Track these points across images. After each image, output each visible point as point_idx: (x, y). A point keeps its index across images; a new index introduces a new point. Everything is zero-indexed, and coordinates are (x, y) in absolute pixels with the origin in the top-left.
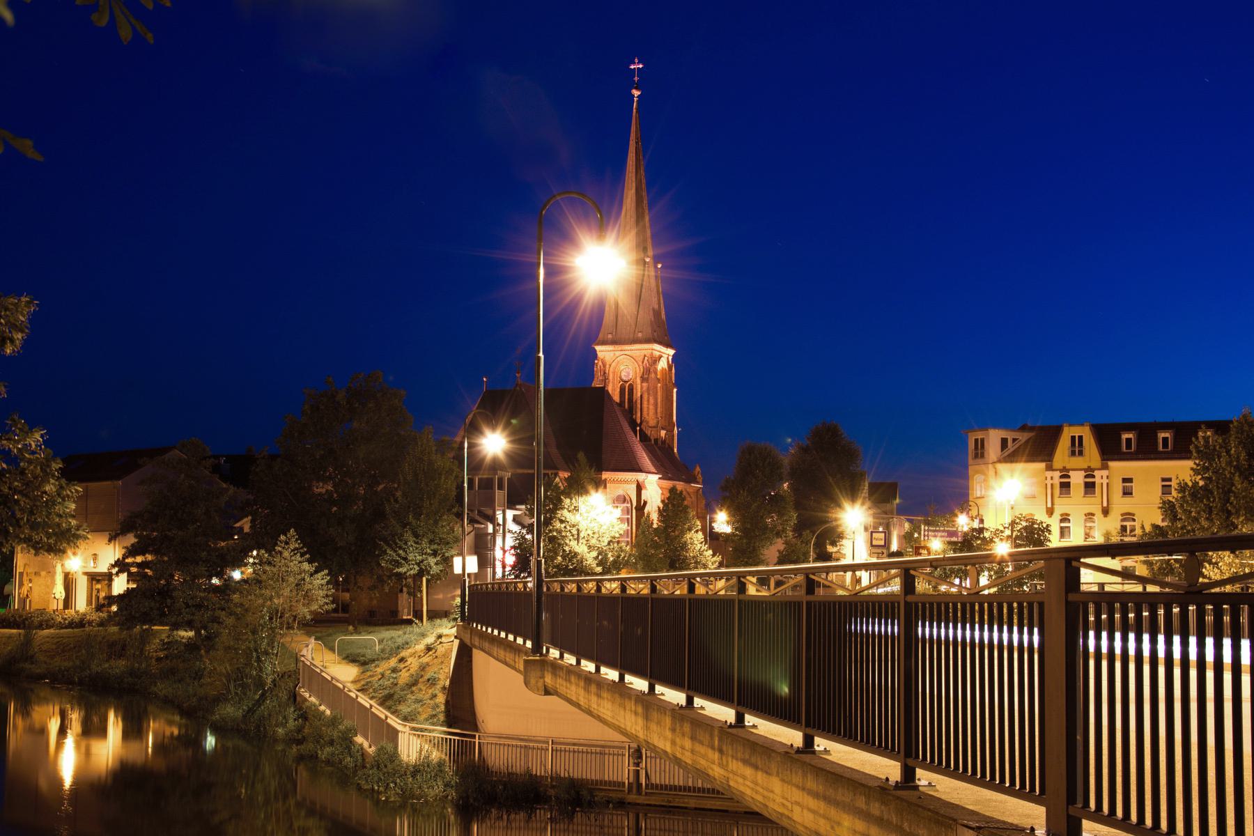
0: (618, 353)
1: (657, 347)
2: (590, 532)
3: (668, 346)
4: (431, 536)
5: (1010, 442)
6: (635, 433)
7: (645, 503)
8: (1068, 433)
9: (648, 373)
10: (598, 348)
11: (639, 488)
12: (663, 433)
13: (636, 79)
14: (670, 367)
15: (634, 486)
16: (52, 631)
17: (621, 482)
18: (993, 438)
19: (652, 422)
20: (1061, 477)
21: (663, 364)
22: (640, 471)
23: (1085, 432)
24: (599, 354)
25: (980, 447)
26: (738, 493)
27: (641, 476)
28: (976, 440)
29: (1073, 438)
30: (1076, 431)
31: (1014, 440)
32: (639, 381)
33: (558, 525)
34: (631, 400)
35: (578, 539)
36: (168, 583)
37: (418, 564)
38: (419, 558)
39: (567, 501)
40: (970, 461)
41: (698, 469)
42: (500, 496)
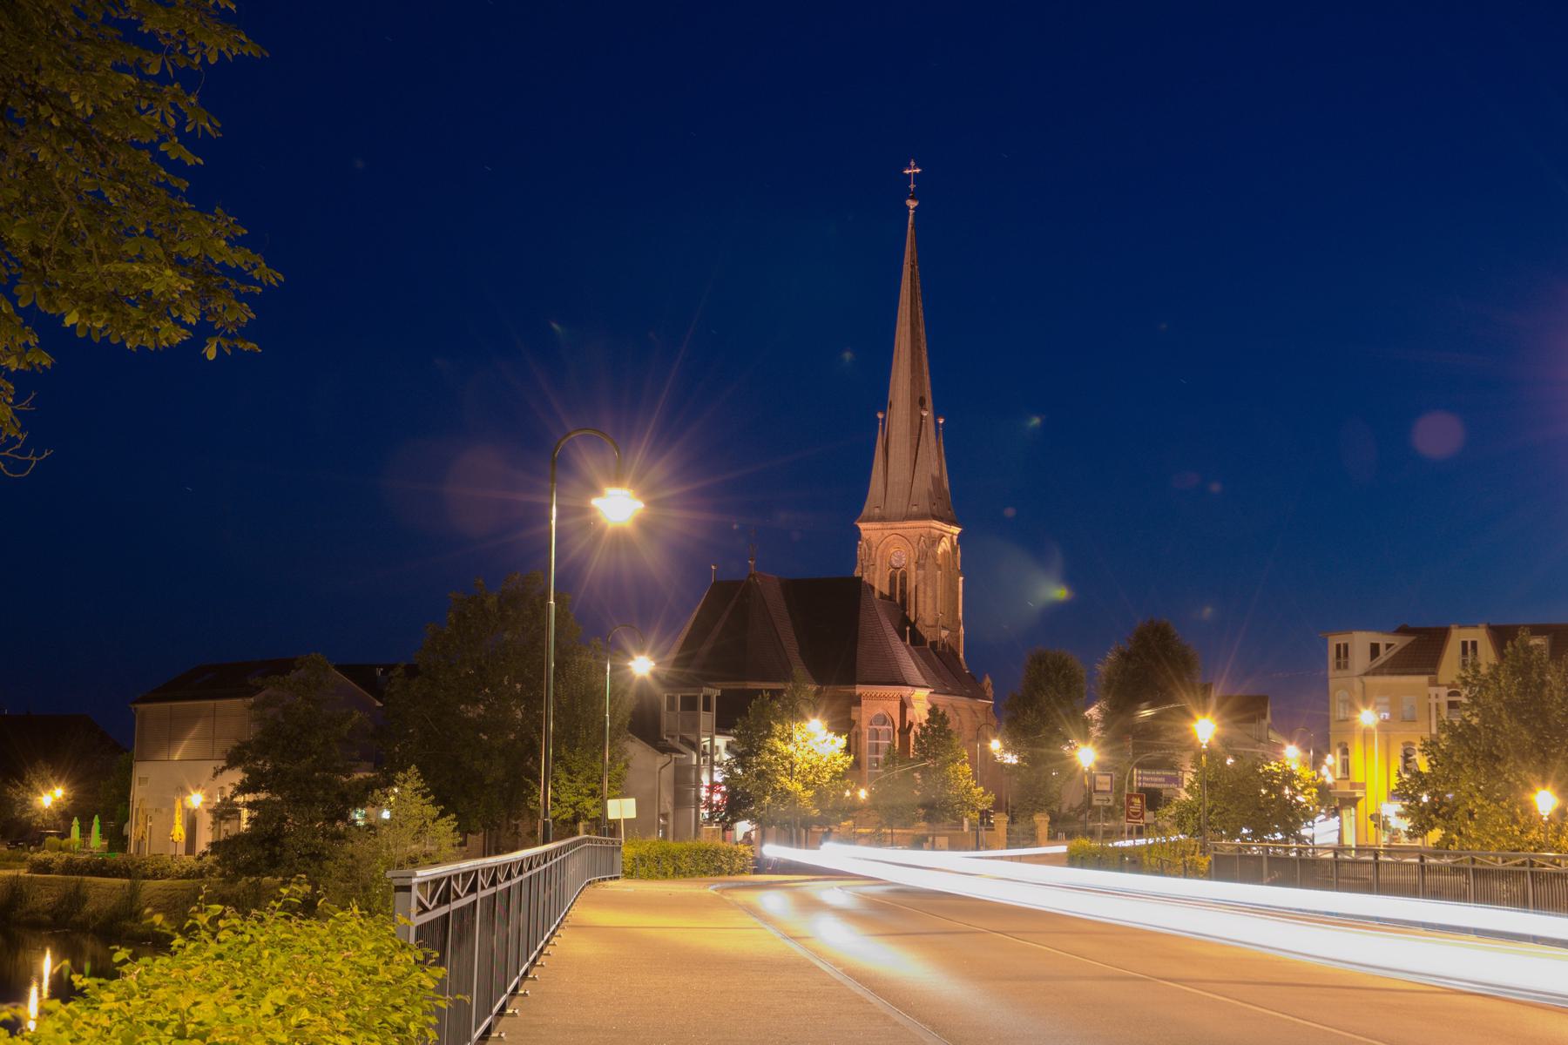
0: (887, 533)
1: (936, 524)
2: (806, 766)
3: (951, 522)
4: (588, 773)
5: (1382, 648)
6: (903, 639)
7: (911, 725)
8: (1457, 636)
9: (924, 557)
10: (862, 526)
11: (904, 705)
12: (944, 633)
13: (912, 186)
14: (954, 549)
15: (897, 703)
16: (166, 881)
17: (880, 698)
18: (1360, 642)
19: (929, 622)
20: (1450, 694)
21: (945, 546)
22: (906, 684)
23: (1480, 635)
24: (864, 534)
25: (1343, 652)
26: (1025, 713)
27: (906, 691)
28: (1338, 646)
29: (1464, 644)
30: (1469, 635)
31: (1388, 646)
32: (913, 567)
33: (767, 757)
34: (903, 592)
35: (791, 775)
36: (280, 828)
37: (573, 807)
38: (574, 799)
39: (779, 727)
40: (1331, 673)
41: (988, 680)
42: (707, 719)
